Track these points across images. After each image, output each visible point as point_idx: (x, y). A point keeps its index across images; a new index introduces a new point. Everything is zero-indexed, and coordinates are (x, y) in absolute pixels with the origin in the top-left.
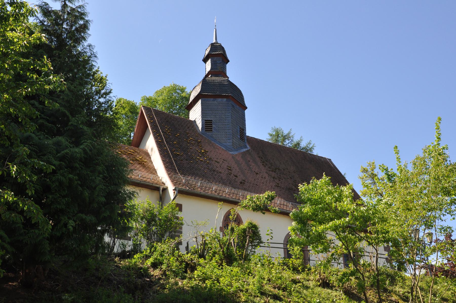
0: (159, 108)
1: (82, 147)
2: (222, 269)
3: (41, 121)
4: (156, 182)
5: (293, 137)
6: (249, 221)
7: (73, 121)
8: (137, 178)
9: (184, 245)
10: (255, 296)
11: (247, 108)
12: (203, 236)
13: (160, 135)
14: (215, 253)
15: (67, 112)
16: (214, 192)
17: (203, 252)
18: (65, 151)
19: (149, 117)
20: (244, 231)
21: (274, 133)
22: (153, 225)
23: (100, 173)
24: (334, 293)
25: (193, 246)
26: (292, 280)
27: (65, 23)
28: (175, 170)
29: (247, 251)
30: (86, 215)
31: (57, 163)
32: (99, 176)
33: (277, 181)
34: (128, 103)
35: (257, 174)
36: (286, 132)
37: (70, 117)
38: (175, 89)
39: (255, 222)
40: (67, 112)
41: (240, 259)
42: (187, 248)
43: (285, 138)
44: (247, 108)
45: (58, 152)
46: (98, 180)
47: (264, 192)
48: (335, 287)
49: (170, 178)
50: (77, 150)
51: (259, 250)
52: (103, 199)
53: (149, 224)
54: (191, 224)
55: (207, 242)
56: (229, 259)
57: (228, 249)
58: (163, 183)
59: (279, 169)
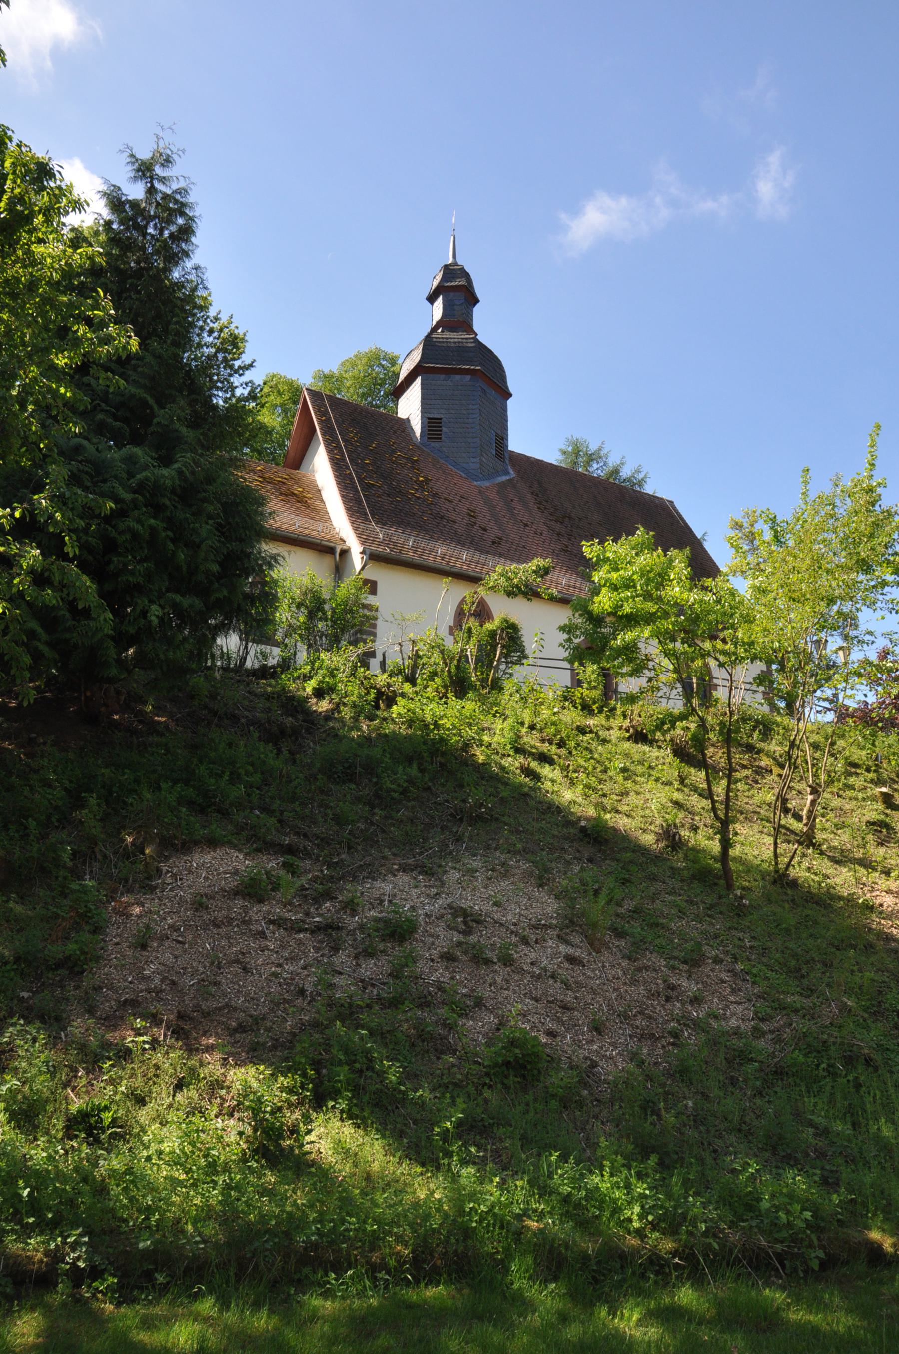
0: (349, 394)
1: (176, 466)
2: (445, 703)
3: (101, 416)
4: (328, 537)
5: (606, 456)
6: (503, 615)
7: (161, 416)
8: (293, 528)
9: (379, 657)
10: (504, 755)
11: (511, 395)
12: (413, 641)
13: (338, 446)
14: (434, 674)
15: (149, 398)
16: (438, 559)
17: (413, 672)
18: (144, 474)
19: (319, 410)
20: (493, 634)
21: (570, 449)
22: (320, 619)
23: (210, 517)
24: (655, 753)
25: (394, 660)
26: (578, 727)
27: (152, 224)
28: (366, 514)
29: (496, 671)
30: (183, 595)
31: (127, 496)
32: (207, 523)
33: (565, 541)
34: (290, 384)
35: (526, 525)
36: (593, 448)
37: (156, 407)
38: (376, 358)
39: (514, 619)
40: (149, 398)
41: (484, 688)
42: (383, 664)
43: (592, 458)
44: (511, 395)
45: (131, 475)
46: (205, 529)
47: (531, 559)
48: (657, 741)
49: (356, 529)
50: (165, 472)
51: (520, 672)
52: (215, 568)
53: (311, 615)
54: (391, 619)
55: (421, 653)
56: (460, 686)
57: (458, 667)
58: (341, 539)
59: (570, 517)
